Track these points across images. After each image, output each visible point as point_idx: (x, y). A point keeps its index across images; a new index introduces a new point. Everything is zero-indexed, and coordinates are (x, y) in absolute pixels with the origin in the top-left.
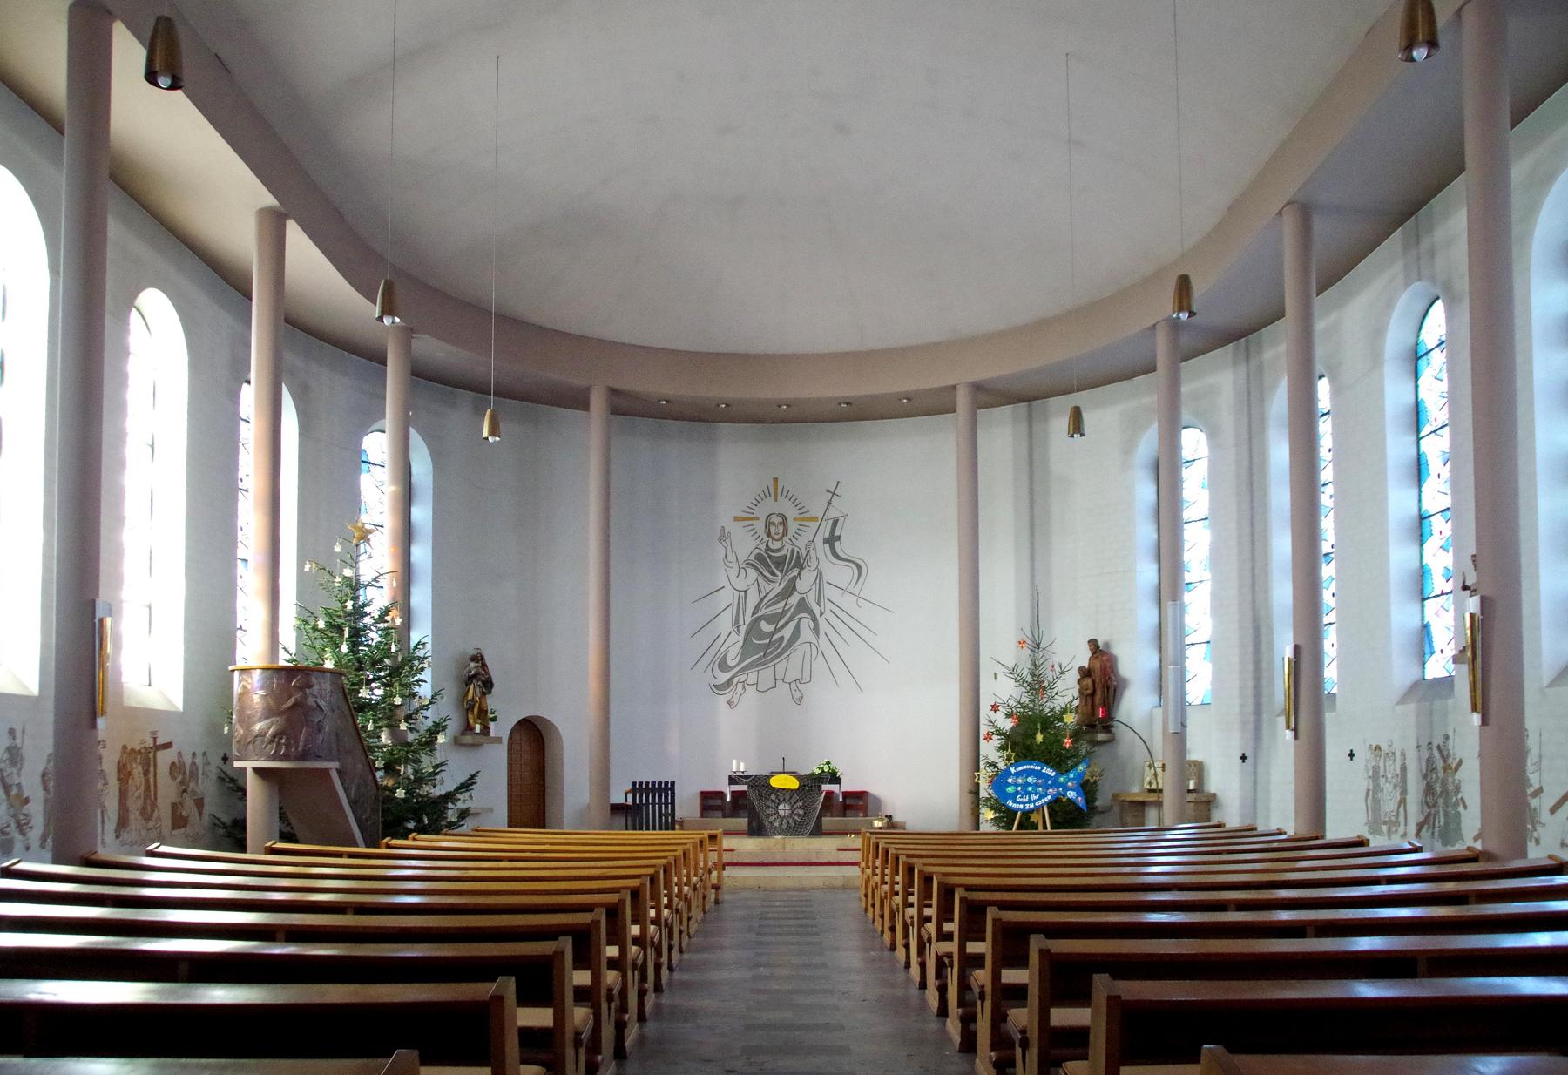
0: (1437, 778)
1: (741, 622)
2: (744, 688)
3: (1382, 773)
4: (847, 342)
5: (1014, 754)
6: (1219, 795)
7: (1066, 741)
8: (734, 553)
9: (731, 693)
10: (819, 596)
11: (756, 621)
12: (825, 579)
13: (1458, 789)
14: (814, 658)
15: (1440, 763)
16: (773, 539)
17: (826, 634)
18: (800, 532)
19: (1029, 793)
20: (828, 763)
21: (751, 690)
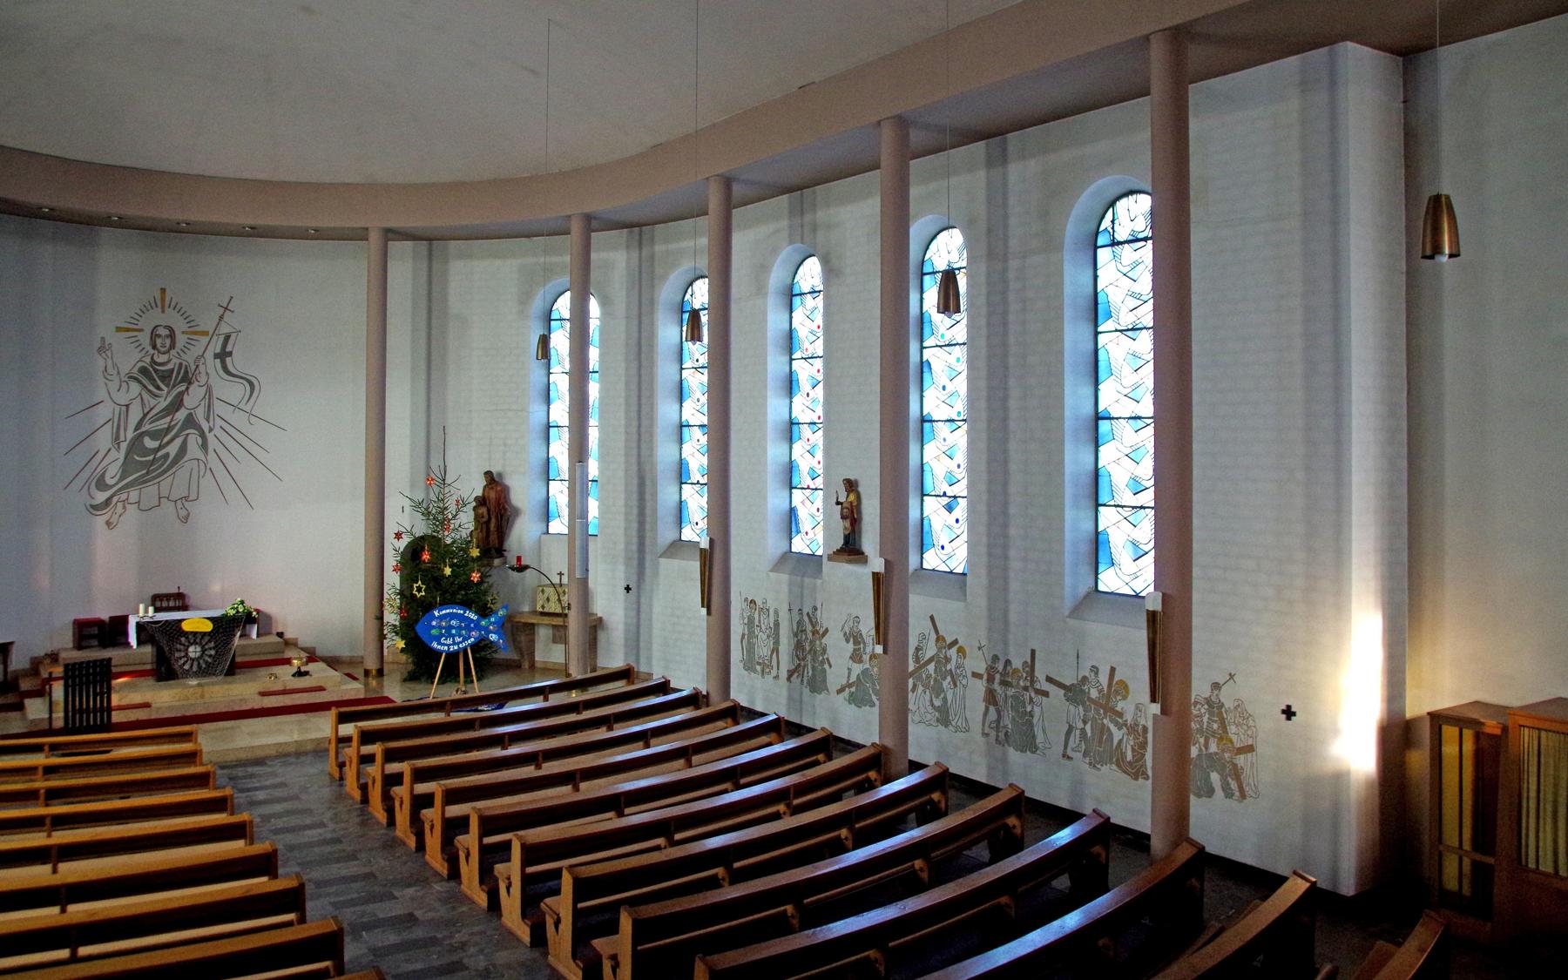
0: (807, 638)
1: (122, 438)
2: (124, 507)
3: (757, 623)
4: (260, 171)
5: (424, 586)
6: (604, 618)
7: (474, 575)
8: (115, 365)
9: (110, 513)
10: (209, 410)
11: (139, 438)
12: (216, 393)
13: (824, 651)
14: (202, 474)
15: (809, 628)
16: (159, 352)
17: (215, 450)
18: (188, 346)
19: (453, 636)
20: (242, 602)
21: (132, 509)
